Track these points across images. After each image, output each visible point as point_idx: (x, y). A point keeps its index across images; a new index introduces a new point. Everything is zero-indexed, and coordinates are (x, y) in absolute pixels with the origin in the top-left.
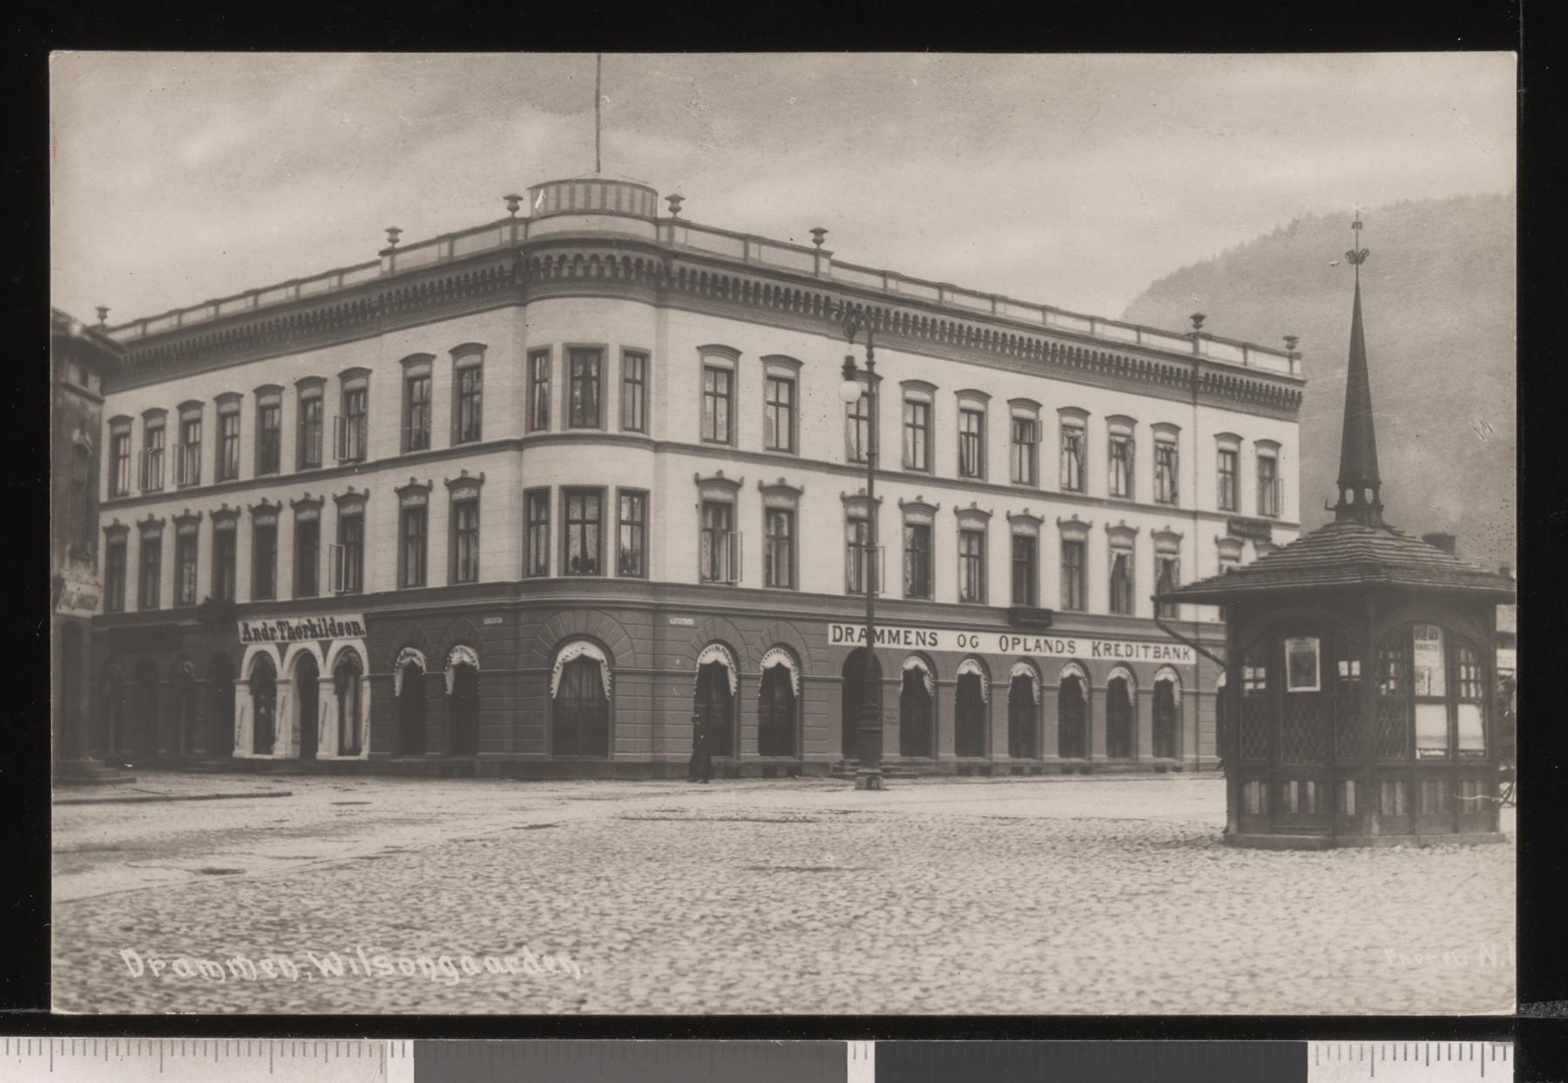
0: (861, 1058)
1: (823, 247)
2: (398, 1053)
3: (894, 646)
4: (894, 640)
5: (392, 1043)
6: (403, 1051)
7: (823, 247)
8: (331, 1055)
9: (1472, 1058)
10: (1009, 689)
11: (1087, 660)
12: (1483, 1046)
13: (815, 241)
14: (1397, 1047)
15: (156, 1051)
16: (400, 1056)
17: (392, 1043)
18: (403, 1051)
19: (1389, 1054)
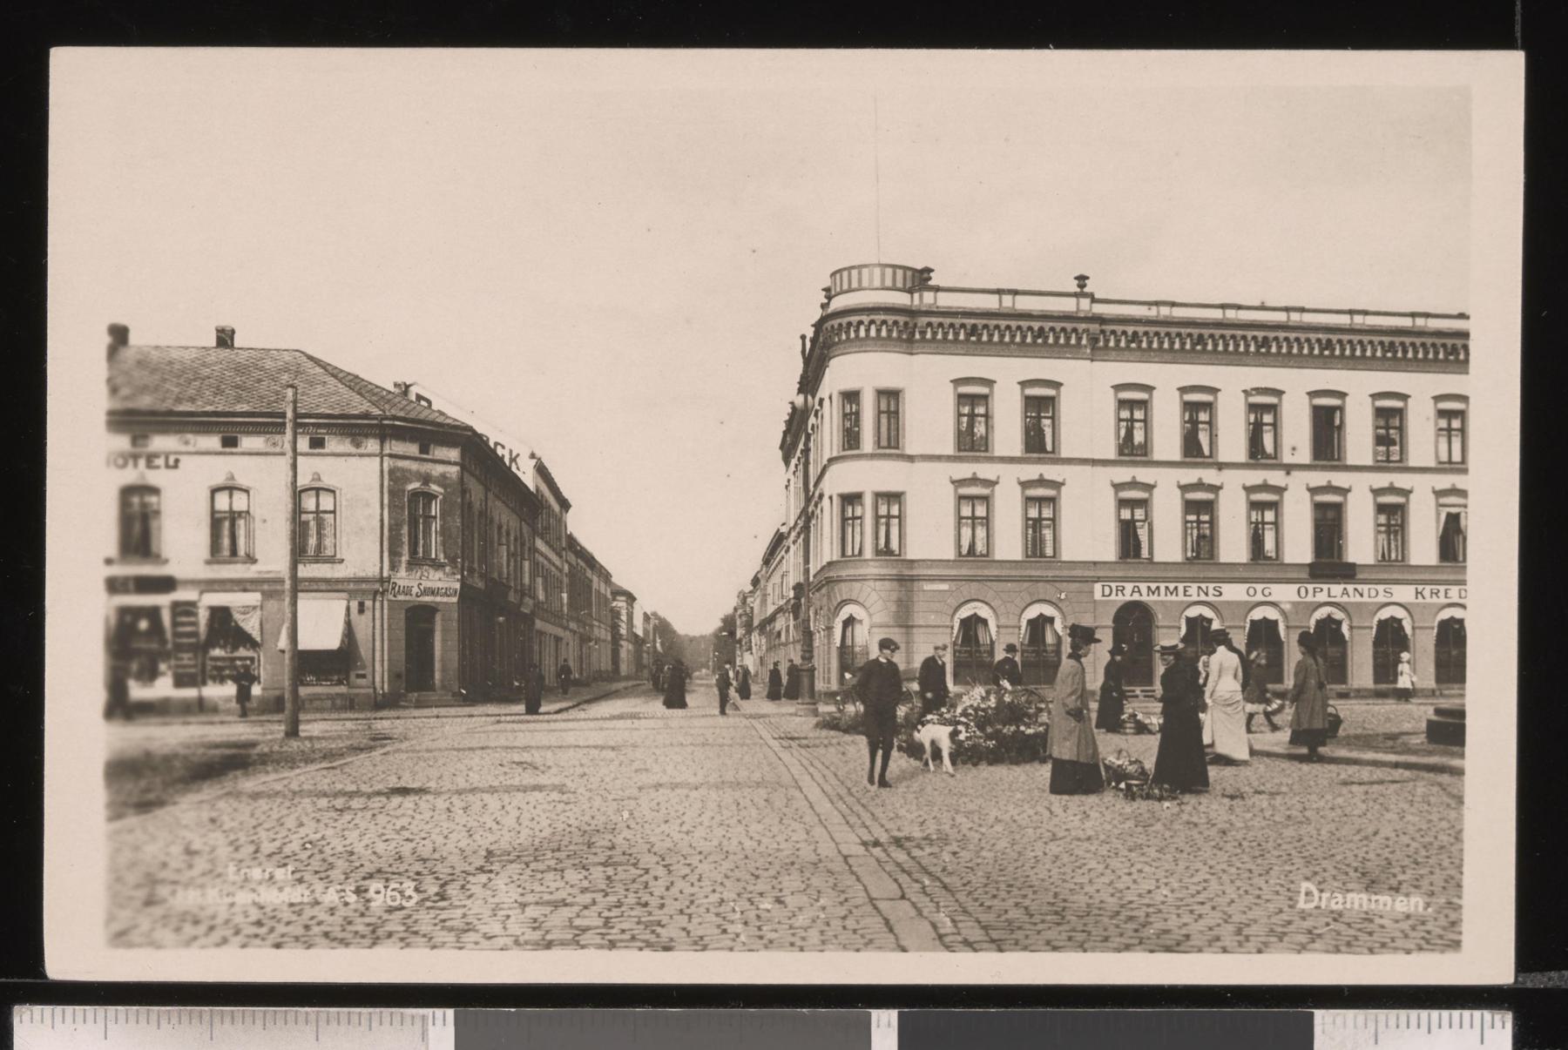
0: (884, 1026)
1: (1086, 290)
2: (439, 1022)
3: (1174, 598)
4: (1153, 593)
5: (434, 1013)
6: (444, 1020)
7: (1086, 290)
8: (375, 1024)
9: (1472, 1026)
10: (1436, 631)
11: (1410, 604)
12: (1482, 1015)
13: (1079, 286)
14: (1422, 1015)
15: (206, 1017)
16: (441, 1024)
17: (434, 1013)
18: (444, 1020)
19: (1392, 1022)
